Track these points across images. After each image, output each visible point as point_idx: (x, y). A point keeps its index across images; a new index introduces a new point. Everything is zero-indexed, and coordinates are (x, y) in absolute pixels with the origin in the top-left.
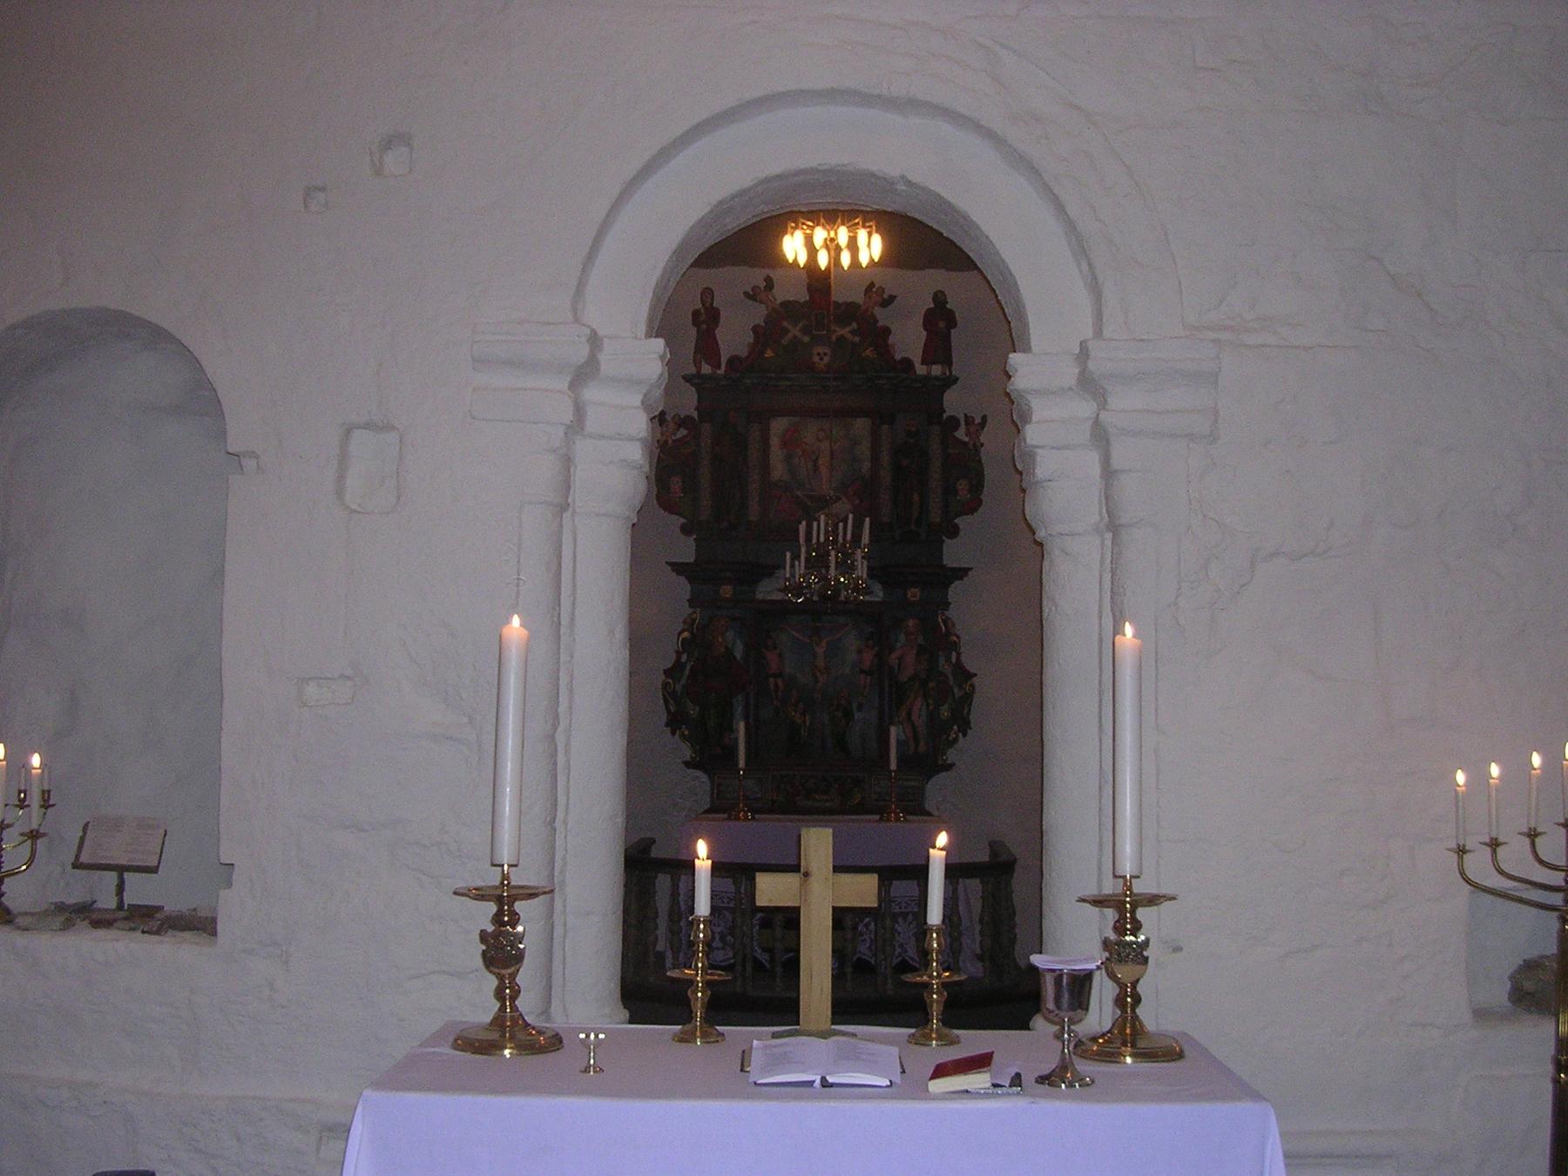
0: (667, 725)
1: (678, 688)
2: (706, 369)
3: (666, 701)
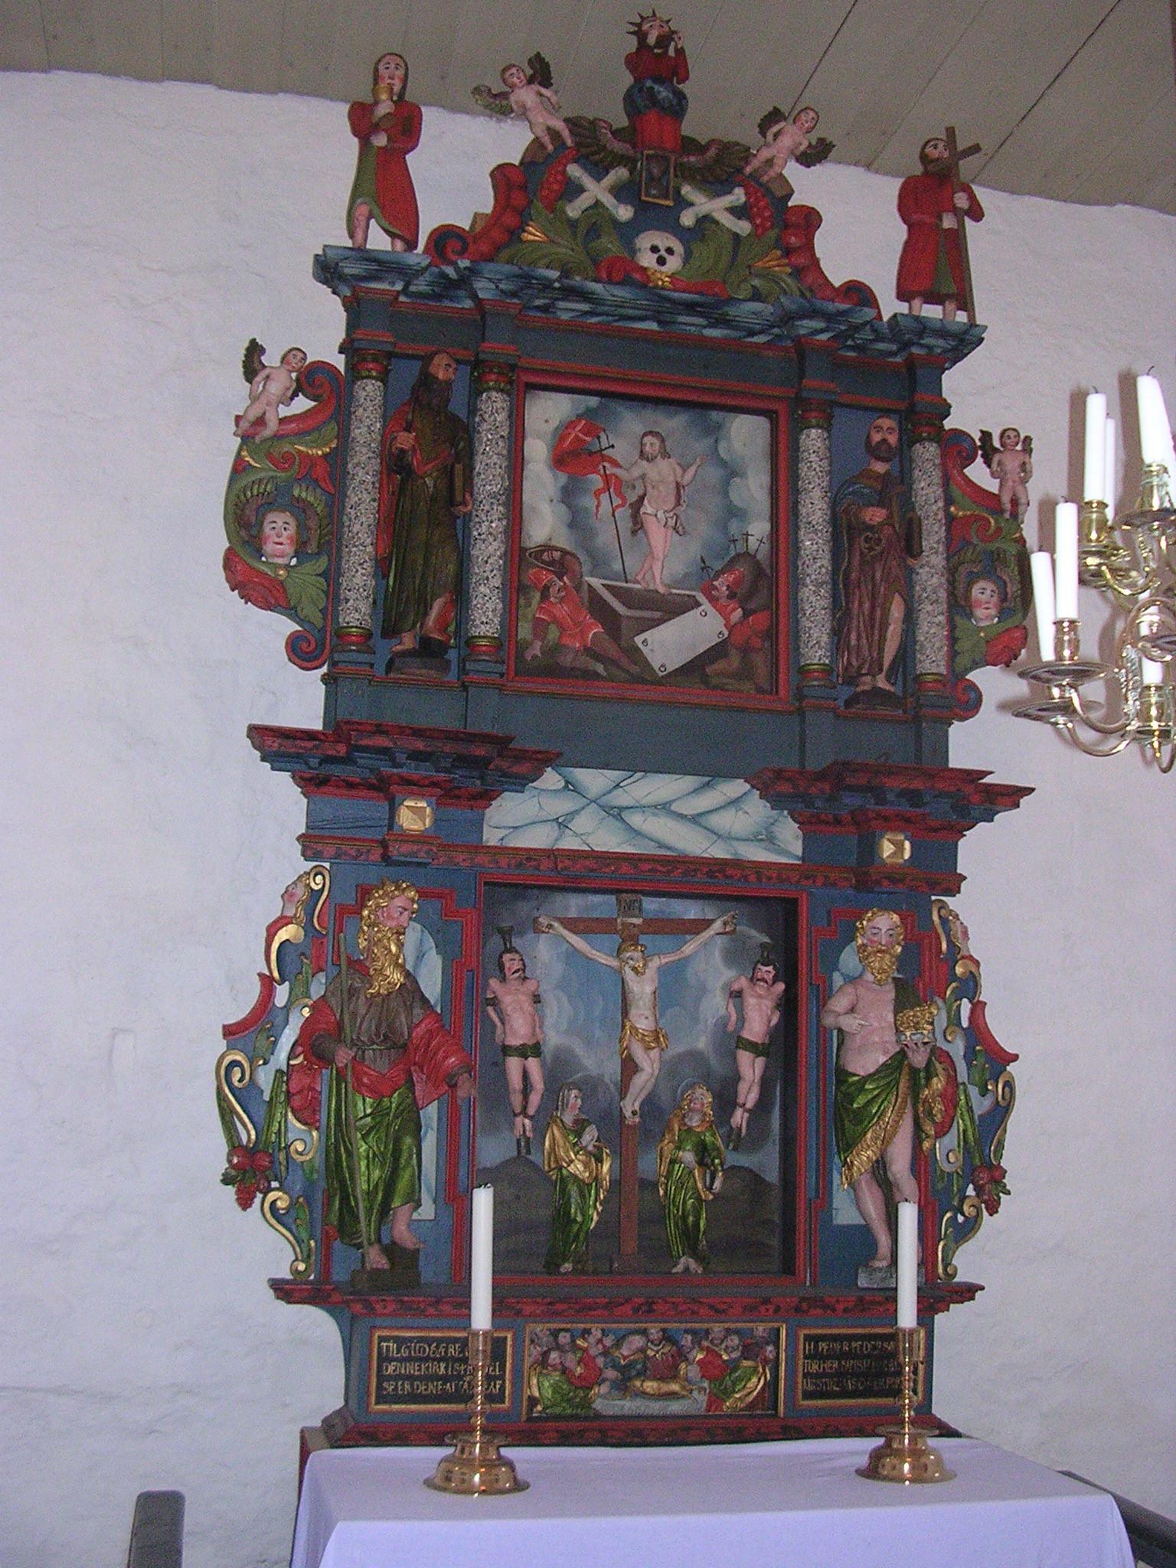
0: (227, 1180)
1: (265, 1078)
2: (378, 240)
3: (226, 1114)
